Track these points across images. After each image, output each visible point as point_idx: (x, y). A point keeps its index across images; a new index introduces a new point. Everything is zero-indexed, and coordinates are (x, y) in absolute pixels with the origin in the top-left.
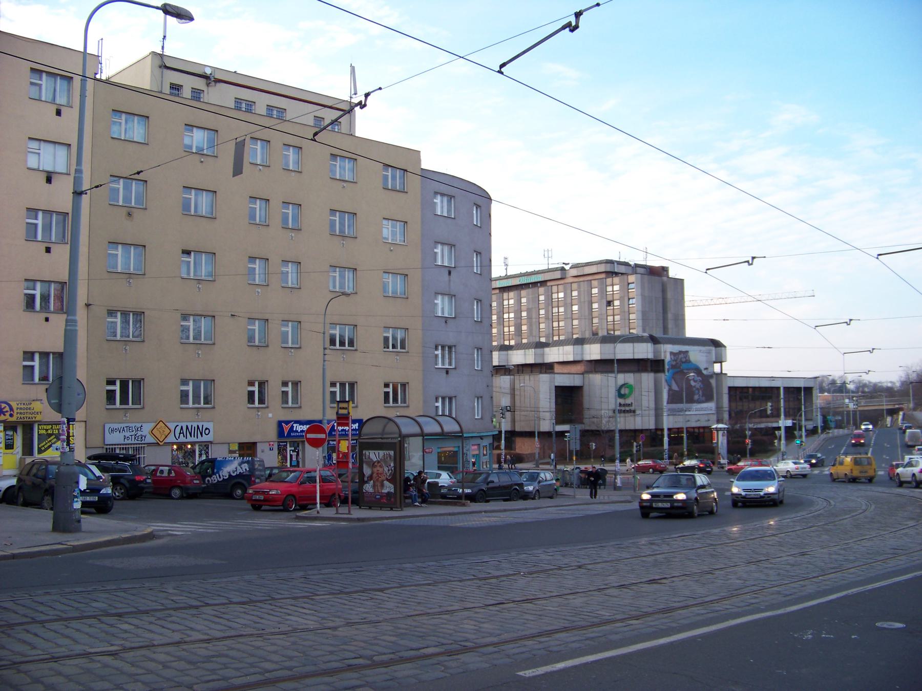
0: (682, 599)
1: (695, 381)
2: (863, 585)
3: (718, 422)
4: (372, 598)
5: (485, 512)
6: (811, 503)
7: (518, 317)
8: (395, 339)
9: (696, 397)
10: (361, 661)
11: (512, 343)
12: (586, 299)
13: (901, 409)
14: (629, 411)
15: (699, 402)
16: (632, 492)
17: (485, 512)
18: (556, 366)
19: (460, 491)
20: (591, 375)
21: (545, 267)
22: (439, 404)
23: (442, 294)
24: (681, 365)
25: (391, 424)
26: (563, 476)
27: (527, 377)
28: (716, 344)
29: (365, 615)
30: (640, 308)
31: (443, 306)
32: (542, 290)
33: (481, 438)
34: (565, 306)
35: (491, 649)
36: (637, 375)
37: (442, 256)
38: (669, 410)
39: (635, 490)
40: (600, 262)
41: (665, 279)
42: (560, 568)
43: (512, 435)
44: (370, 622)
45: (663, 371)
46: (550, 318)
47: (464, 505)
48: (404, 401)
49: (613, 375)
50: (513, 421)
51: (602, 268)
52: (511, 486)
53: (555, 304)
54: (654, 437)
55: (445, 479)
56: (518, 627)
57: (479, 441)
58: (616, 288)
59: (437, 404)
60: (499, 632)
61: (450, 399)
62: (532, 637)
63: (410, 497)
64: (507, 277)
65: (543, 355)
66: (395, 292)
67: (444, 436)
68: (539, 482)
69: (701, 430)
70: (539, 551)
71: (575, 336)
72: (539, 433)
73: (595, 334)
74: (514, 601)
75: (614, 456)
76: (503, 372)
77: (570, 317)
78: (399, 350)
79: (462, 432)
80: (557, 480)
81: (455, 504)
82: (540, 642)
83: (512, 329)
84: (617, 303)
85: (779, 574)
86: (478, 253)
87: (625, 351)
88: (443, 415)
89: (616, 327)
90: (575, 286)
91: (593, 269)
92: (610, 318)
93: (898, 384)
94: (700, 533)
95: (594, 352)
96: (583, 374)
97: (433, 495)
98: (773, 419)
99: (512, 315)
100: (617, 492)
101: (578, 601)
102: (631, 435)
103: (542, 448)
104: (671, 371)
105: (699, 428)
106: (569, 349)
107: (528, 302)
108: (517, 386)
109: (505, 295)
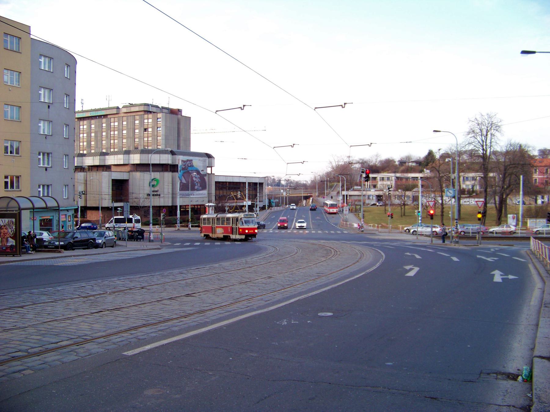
0: (208, 305)
1: (196, 178)
2: (306, 294)
3: (209, 202)
4: (17, 313)
5: (74, 256)
6: (266, 249)
7: (89, 136)
8: (12, 146)
9: (196, 187)
10: (20, 354)
11: (85, 152)
12: (132, 127)
13: (311, 196)
14: (157, 195)
15: (197, 190)
16: (160, 243)
17: (74, 256)
18: (112, 166)
19: (57, 243)
20: (134, 173)
21: (107, 106)
22: (41, 189)
23: (43, 120)
24: (188, 168)
25: (13, 201)
26: (118, 234)
27: (94, 173)
28: (209, 156)
29: (16, 324)
30: (164, 134)
31: (44, 128)
32: (104, 120)
33: (68, 210)
34: (118, 130)
35: (102, 340)
36: (162, 173)
37: (44, 96)
38: (180, 194)
39: (162, 242)
40: (141, 105)
41: (180, 116)
42: (130, 289)
43: (85, 209)
44: (20, 328)
45: (177, 171)
46: (109, 137)
47: (60, 252)
48: (18, 187)
49: (148, 173)
50: (86, 201)
51: (142, 108)
52: (88, 240)
53: (112, 129)
54: (172, 210)
55: (46, 236)
56: (116, 326)
57: (66, 212)
58: (150, 121)
59: (39, 190)
60: (105, 329)
61: (48, 186)
62: (126, 331)
63: (25, 248)
64: (83, 112)
65: (105, 160)
66: (12, 117)
67: (47, 209)
68: (105, 237)
69: (199, 207)
70: (115, 279)
71: (124, 149)
72: (102, 208)
73: (136, 148)
74: (108, 310)
75: (149, 222)
76: (79, 170)
77: (121, 137)
78: (15, 154)
79: (59, 207)
80: (115, 236)
81: (54, 252)
82: (132, 334)
83: (85, 143)
84: (150, 130)
85: (259, 289)
86: (67, 95)
87: (156, 159)
88: (48, 196)
89: (149, 144)
90: (125, 119)
91: (137, 109)
92: (146, 139)
93: (309, 182)
94: (208, 266)
95: (136, 159)
96: (129, 172)
97: (40, 246)
98: (241, 201)
99: (85, 135)
100: (151, 243)
101: (147, 308)
102: (158, 209)
103: (104, 217)
104: (182, 171)
105: (197, 205)
106: (121, 156)
107: (95, 127)
108: (88, 179)
109: (81, 123)
